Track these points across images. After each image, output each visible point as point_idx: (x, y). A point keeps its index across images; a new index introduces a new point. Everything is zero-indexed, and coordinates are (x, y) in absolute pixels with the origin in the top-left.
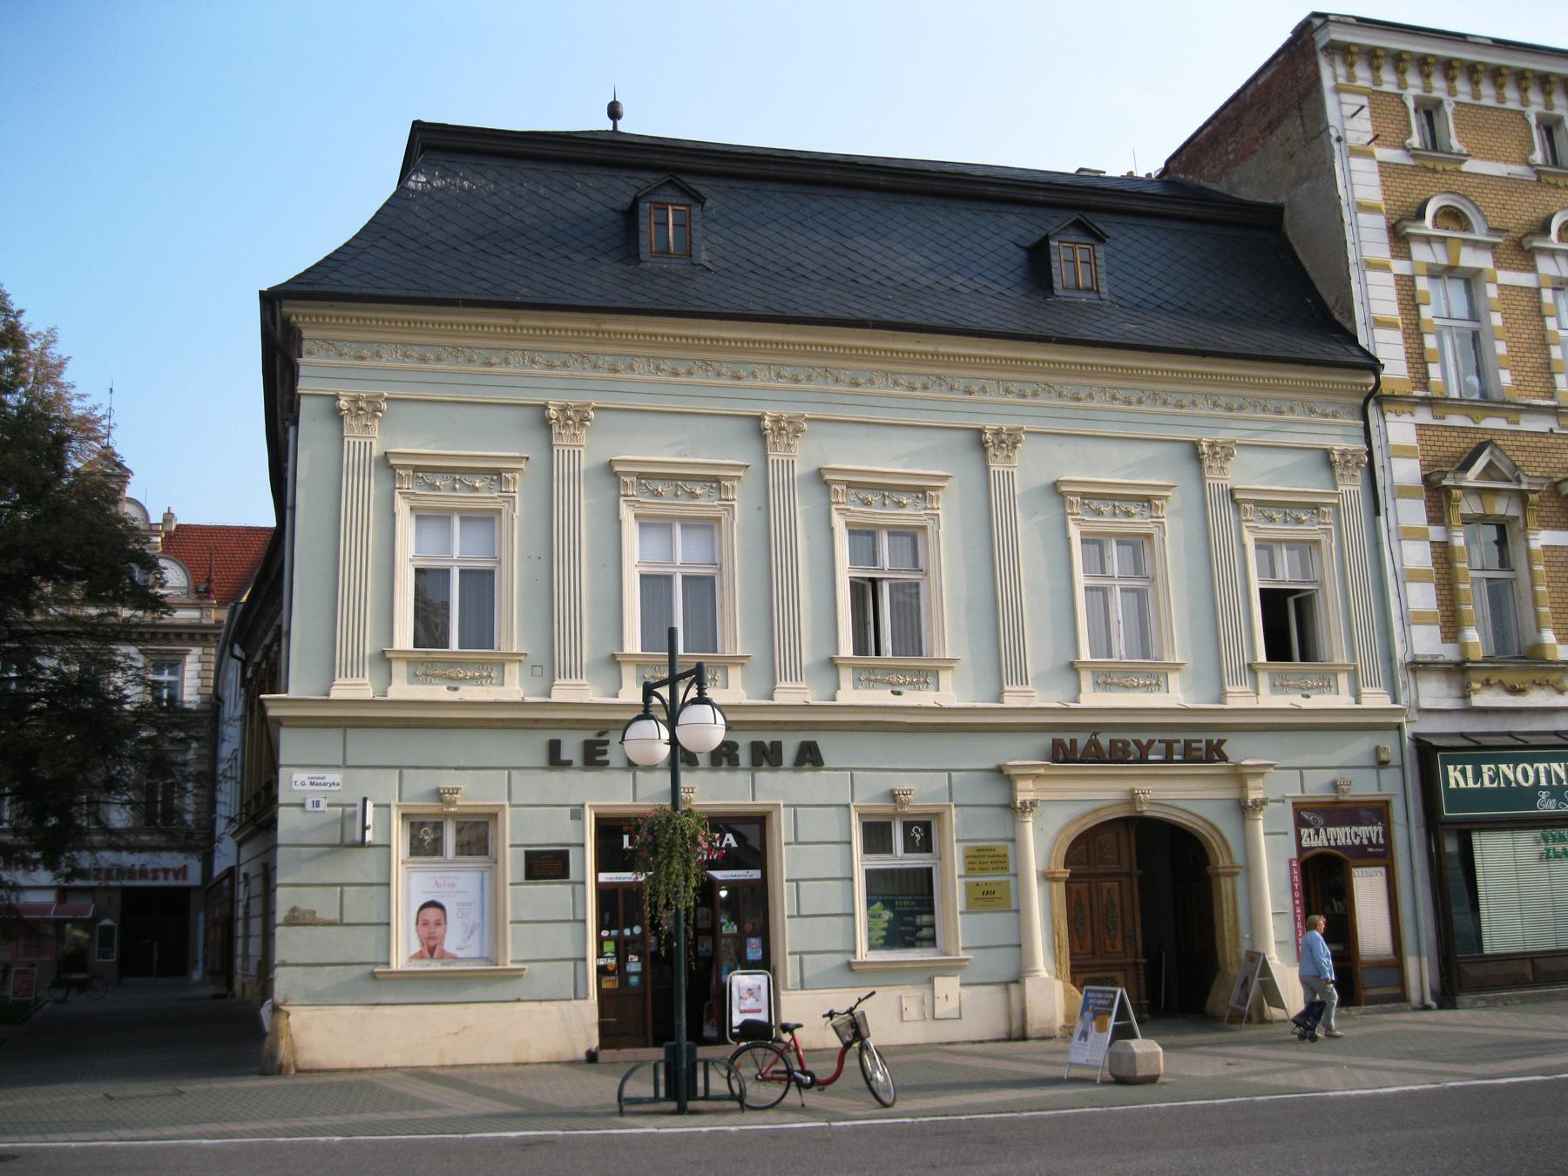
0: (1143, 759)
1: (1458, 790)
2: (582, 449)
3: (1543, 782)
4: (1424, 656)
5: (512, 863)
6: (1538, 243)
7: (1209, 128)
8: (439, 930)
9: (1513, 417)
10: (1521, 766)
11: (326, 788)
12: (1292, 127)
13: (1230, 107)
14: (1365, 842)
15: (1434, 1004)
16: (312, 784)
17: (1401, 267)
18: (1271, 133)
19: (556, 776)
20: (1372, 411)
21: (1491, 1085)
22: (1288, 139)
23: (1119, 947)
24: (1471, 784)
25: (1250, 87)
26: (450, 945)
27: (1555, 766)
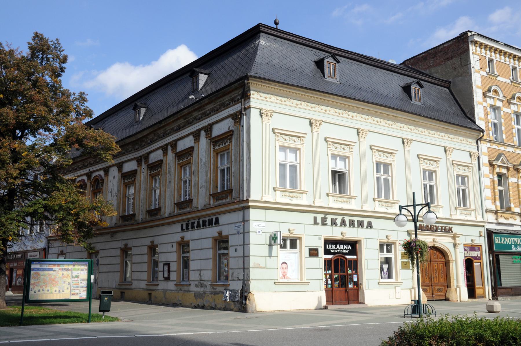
0: (436, 231)
1: (497, 244)
2: (270, 124)
3: (513, 243)
4: (489, 208)
5: (306, 252)
6: (512, 101)
7: (423, 55)
8: (286, 270)
9: (505, 147)
10: (509, 238)
11: (262, 227)
12: (456, 61)
13: (432, 50)
14: (477, 256)
15: (492, 299)
16: (258, 226)
17: (485, 104)
18: (448, 61)
19: (316, 226)
20: (479, 142)
21: (200, 334)
22: (455, 64)
23: (428, 281)
24: (500, 243)
25: (441, 46)
26: (289, 275)
27: (515, 239)
